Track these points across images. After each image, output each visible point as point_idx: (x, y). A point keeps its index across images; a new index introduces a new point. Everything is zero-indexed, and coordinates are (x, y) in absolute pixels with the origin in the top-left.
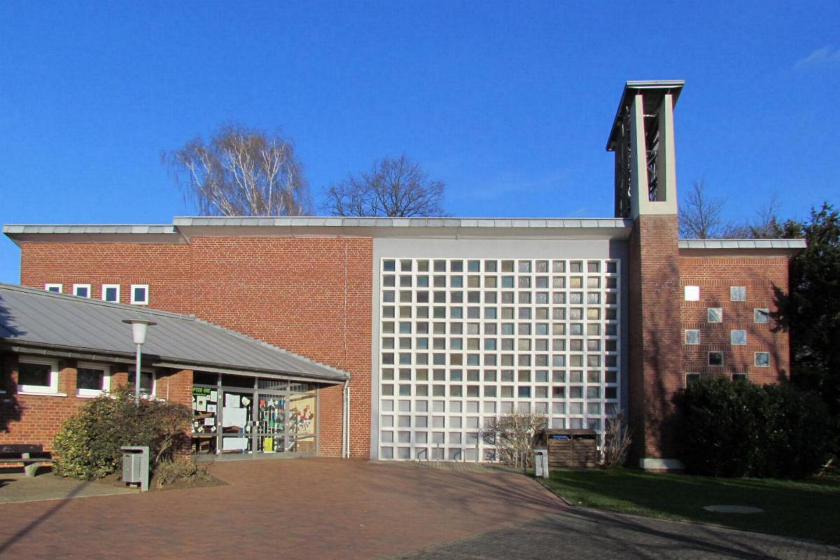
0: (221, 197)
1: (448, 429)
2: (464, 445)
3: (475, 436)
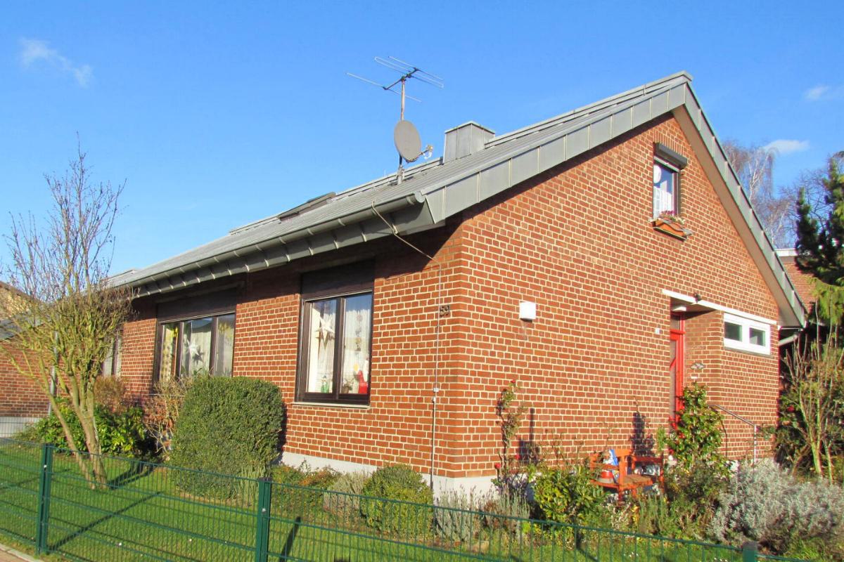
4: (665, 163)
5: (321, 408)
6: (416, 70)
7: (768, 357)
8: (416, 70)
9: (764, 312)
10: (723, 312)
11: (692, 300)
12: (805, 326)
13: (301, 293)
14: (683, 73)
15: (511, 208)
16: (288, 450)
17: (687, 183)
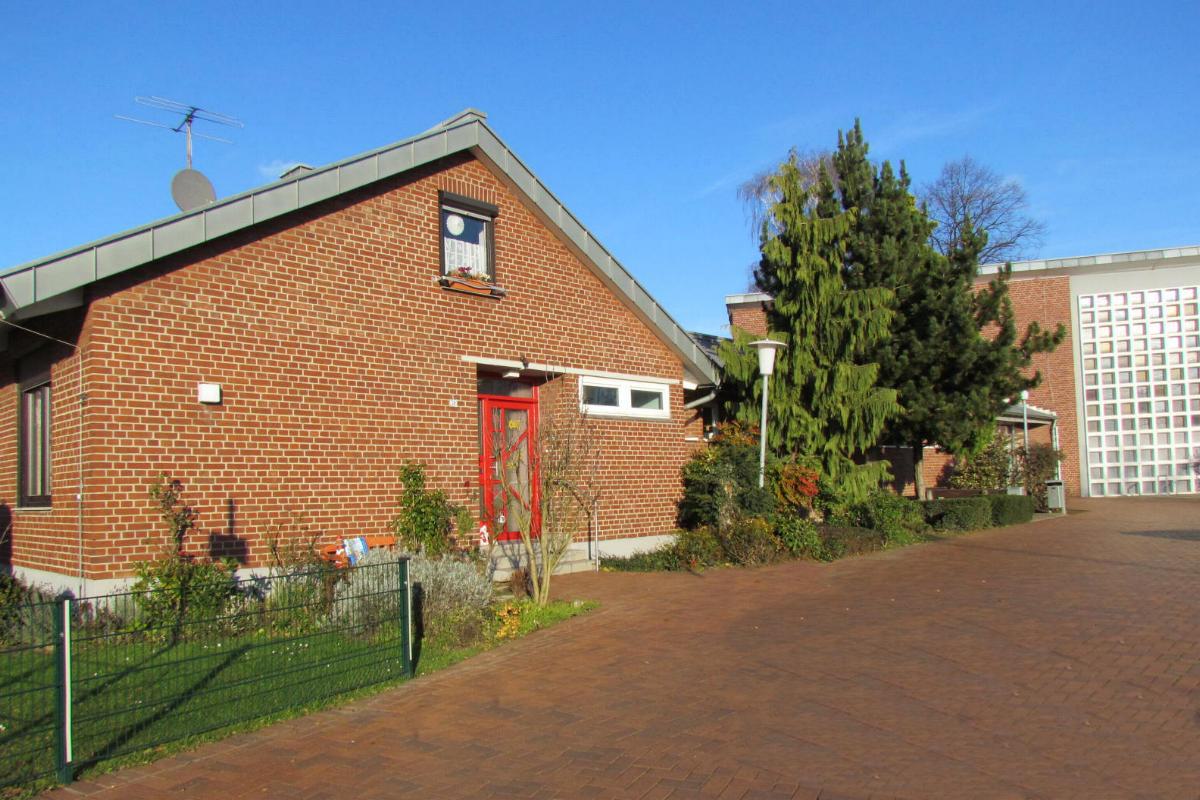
0: (858, 343)
1: (1157, 462)
2: (1174, 477)
3: (1185, 468)
4: (466, 213)
5: (36, 512)
6: (195, 110)
7: (667, 421)
8: (195, 110)
9: (657, 371)
10: (577, 376)
11: (519, 365)
12: (718, 383)
13: (18, 382)
14: (469, 110)
15: (180, 281)
16: (17, 564)
17: (502, 232)
